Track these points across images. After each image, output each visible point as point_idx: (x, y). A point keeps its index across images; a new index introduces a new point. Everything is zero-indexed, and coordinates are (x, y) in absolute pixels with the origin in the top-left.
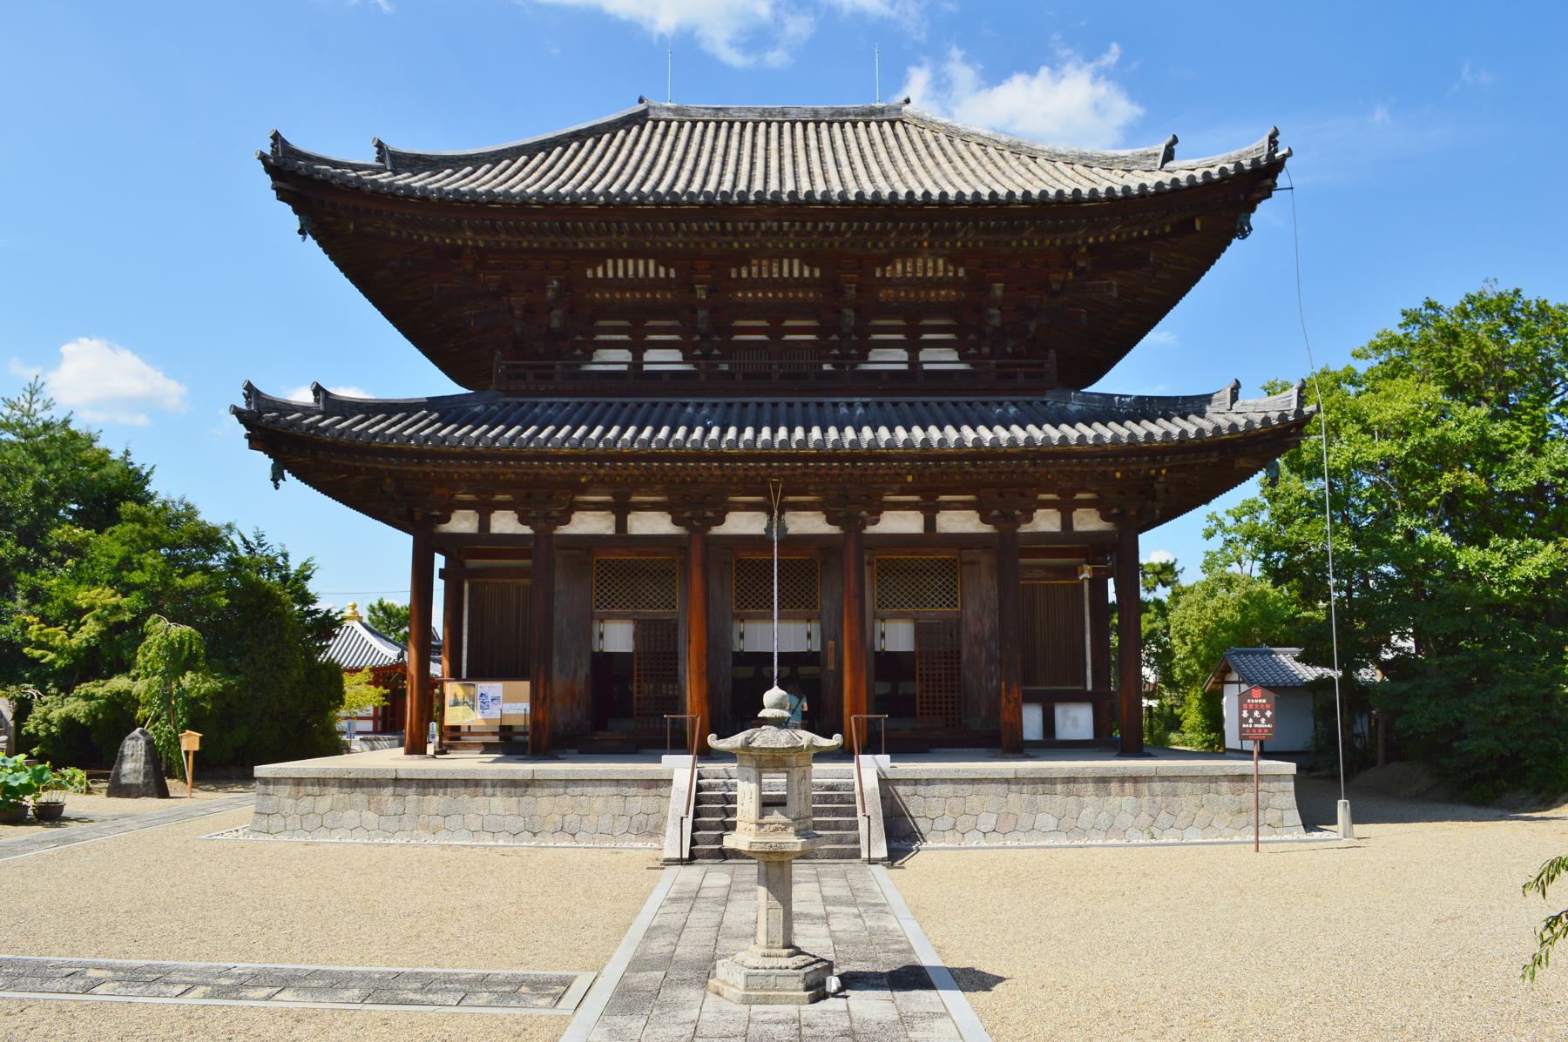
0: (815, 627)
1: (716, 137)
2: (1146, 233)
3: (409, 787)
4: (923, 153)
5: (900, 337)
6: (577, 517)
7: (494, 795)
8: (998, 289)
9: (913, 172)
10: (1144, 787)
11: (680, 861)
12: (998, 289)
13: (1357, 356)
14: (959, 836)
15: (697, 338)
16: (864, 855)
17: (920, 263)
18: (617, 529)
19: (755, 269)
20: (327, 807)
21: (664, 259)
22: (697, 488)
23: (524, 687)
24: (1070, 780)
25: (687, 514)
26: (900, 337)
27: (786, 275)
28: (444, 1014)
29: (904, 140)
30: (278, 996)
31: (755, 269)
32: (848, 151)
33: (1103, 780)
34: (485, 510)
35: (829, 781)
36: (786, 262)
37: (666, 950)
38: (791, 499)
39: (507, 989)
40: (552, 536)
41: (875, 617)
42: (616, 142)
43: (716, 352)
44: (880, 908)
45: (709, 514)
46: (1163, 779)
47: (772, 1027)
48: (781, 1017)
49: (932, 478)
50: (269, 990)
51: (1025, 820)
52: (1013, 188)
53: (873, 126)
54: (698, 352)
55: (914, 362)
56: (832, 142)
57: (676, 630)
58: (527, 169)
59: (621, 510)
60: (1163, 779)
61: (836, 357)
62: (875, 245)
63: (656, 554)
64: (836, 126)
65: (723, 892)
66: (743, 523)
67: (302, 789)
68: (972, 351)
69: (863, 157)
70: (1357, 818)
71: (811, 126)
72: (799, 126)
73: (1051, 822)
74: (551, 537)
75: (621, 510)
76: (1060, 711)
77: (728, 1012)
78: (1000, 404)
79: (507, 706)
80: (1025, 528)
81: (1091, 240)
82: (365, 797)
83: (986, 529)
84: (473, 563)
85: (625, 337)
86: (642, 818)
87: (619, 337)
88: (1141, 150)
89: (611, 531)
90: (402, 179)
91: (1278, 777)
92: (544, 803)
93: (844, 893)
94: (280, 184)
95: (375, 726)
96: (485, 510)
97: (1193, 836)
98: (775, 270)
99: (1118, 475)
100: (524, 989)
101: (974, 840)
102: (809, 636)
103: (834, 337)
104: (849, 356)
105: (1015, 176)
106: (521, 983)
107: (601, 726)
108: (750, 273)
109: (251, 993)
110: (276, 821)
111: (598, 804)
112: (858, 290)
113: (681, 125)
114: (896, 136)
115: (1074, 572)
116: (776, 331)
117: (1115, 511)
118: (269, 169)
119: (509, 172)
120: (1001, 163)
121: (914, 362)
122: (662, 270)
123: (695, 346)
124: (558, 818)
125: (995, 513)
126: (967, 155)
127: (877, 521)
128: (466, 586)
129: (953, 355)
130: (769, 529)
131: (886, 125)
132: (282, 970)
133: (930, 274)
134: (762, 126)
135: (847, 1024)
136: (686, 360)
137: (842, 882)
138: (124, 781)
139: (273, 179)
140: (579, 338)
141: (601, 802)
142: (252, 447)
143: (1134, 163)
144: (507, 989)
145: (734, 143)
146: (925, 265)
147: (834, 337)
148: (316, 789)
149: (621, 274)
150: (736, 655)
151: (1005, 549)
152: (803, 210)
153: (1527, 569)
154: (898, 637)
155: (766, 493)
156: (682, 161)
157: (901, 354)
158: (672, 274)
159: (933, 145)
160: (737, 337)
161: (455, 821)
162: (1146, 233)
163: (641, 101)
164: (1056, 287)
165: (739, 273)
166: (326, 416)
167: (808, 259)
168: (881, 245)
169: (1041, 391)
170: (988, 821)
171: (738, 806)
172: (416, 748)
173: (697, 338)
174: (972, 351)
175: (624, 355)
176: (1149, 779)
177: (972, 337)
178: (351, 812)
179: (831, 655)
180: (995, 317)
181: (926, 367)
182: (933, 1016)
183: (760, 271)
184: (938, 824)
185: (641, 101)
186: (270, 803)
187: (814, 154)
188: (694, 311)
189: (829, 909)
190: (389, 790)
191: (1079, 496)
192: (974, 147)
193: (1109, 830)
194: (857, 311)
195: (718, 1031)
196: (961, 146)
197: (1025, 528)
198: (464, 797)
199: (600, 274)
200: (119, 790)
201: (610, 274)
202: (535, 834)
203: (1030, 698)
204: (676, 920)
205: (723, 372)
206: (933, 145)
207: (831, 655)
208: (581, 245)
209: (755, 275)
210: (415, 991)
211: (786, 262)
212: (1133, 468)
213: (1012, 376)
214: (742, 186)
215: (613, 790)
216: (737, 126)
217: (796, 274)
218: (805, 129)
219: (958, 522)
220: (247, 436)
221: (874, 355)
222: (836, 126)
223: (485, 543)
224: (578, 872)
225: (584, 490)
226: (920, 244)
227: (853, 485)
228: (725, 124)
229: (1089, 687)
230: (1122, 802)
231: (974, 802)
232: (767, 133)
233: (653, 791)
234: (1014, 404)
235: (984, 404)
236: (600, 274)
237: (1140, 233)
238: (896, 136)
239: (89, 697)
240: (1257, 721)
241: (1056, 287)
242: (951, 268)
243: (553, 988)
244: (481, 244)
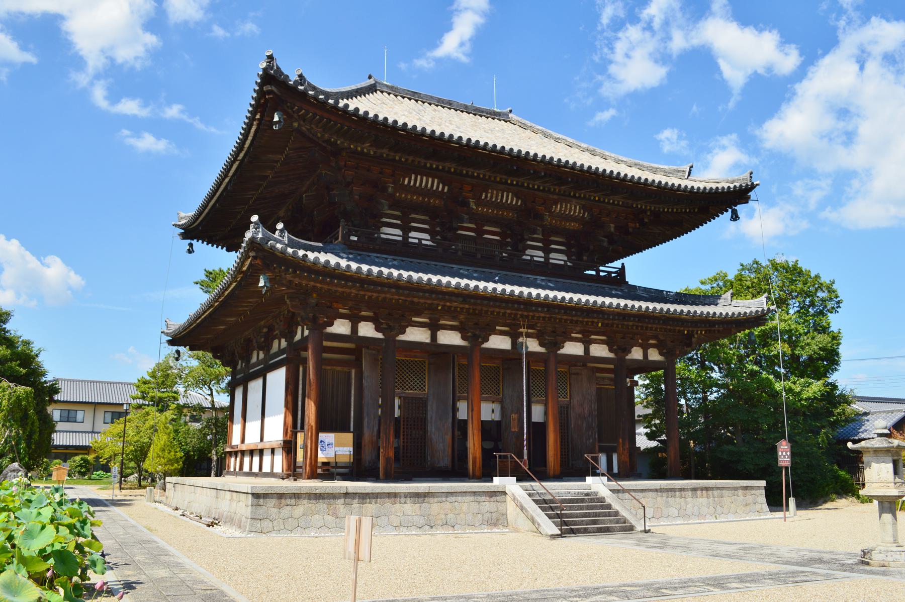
3: (354, 498)
5: (540, 244)
6: (409, 330)
7: (405, 503)
10: (710, 493)
13: (702, 283)
20: (301, 513)
23: (349, 437)
24: (682, 490)
26: (540, 244)
33: (694, 490)
34: (355, 321)
35: (586, 491)
40: (395, 341)
46: (718, 488)
57: (426, 406)
59: (434, 328)
60: (718, 488)
63: (415, 357)
67: (283, 501)
70: (799, 506)
75: (434, 328)
79: (337, 449)
82: (325, 506)
85: (399, 222)
86: (489, 515)
88: (675, 167)
89: (428, 341)
91: (759, 488)
92: (435, 507)
96: (355, 321)
97: (731, 517)
102: (493, 411)
108: (486, 197)
110: (266, 524)
111: (465, 507)
122: (441, 186)
123: (437, 233)
124: (443, 516)
141: (466, 505)
148: (293, 501)
153: (808, 393)
160: (486, 236)
161: (383, 520)
163: (370, 77)
167: (517, 195)
176: (712, 489)
178: (317, 516)
183: (492, 197)
185: (370, 77)
190: (341, 501)
193: (699, 516)
198: (388, 504)
199: (406, 182)
202: (432, 527)
203: (602, 450)
215: (472, 498)
230: (702, 500)
233: (493, 499)
236: (406, 182)
241: (630, 230)
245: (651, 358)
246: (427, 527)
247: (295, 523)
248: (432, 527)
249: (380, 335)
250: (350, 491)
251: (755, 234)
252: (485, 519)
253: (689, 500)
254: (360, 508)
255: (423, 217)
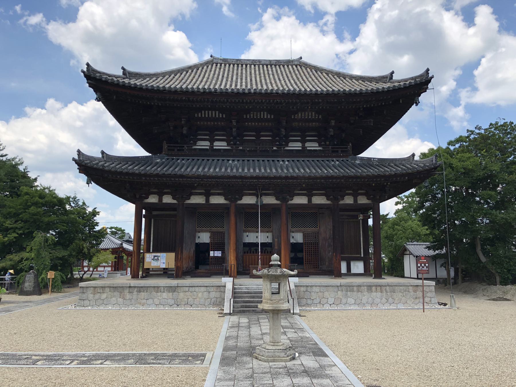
0: (270, 235)
1: (238, 69)
2: (383, 104)
4: (308, 76)
5: (299, 138)
6: (192, 197)
8: (333, 123)
9: (305, 83)
11: (230, 314)
12: (333, 123)
14: (322, 306)
15: (232, 138)
16: (292, 312)
17: (307, 114)
18: (206, 202)
19: (252, 115)
21: (221, 111)
22: (234, 187)
25: (230, 197)
27: (262, 117)
28: (161, 369)
29: (301, 72)
30: (105, 363)
31: (252, 115)
32: (282, 75)
36: (262, 113)
37: (234, 344)
38: (264, 192)
39: (184, 358)
41: (291, 232)
42: (204, 71)
43: (238, 143)
44: (302, 330)
45: (237, 197)
47: (279, 370)
48: (280, 366)
49: (310, 186)
50: (101, 361)
51: (344, 301)
52: (340, 88)
53: (290, 67)
54: (232, 143)
55: (304, 147)
56: (277, 72)
58: (175, 79)
61: (277, 145)
62: (293, 108)
64: (277, 66)
65: (247, 324)
66: (248, 200)
68: (323, 143)
69: (288, 77)
71: (269, 66)
72: (265, 66)
73: (353, 302)
74: (183, 204)
75: (208, 195)
76: (352, 264)
77: (262, 365)
78: (333, 161)
80: (341, 202)
81: (365, 106)
83: (329, 202)
84: (155, 213)
85: (208, 137)
87: (205, 137)
89: (204, 202)
90: (133, 82)
93: (288, 324)
94: (89, 81)
95: (112, 269)
97: (400, 306)
98: (259, 115)
99: (374, 185)
100: (190, 358)
101: (327, 307)
102: (268, 237)
103: (277, 138)
104: (282, 145)
105: (339, 84)
106: (189, 356)
107: (197, 268)
108: (250, 116)
109: (95, 362)
110: (87, 302)
112: (286, 123)
113: (225, 65)
114: (298, 70)
115: (357, 217)
116: (258, 136)
117: (372, 197)
118: (86, 76)
119: (169, 80)
120: (334, 80)
121: (304, 147)
122: (221, 115)
124: (186, 300)
125: (332, 197)
126: (322, 77)
127: (292, 200)
128: (152, 220)
129: (317, 145)
130: (257, 202)
131: (294, 66)
132: (103, 354)
133: (310, 117)
134: (253, 66)
135: (303, 368)
136: (228, 145)
137: (286, 321)
138: (25, 289)
139: (87, 80)
140: (192, 137)
142: (80, 172)
143: (379, 80)
144: (184, 358)
145: (244, 72)
146: (308, 114)
147: (277, 138)
149: (207, 116)
150: (244, 244)
151: (333, 210)
152: (269, 95)
154: (298, 237)
155: (256, 190)
156: (227, 78)
157: (299, 144)
158: (224, 116)
159: (311, 73)
160: (262, 138)
161: (150, 301)
162: (383, 104)
164: (352, 122)
165: (247, 116)
166: (106, 162)
167: (270, 112)
168: (295, 107)
169: (347, 156)
170: (331, 301)
171: (263, 295)
172: (135, 276)
173: (232, 138)
174: (323, 143)
175: (207, 143)
177: (323, 138)
178: (114, 299)
179: (276, 244)
180: (332, 132)
181: (308, 148)
182: (331, 366)
183: (253, 116)
184: (315, 301)
186: (84, 296)
187: (271, 76)
188: (231, 129)
189: (285, 330)
191: (360, 192)
192: (324, 74)
194: (285, 129)
195: (260, 371)
196: (320, 74)
197: (341, 202)
199: (200, 116)
200: (23, 293)
201: (203, 116)
202: (178, 305)
203: (343, 259)
204: (235, 334)
205: (240, 150)
206: (311, 73)
207: (276, 244)
208: (194, 106)
209: (252, 117)
210: (152, 359)
211: (262, 113)
212: (379, 182)
213: (337, 151)
214: (249, 87)
216: (244, 66)
217: (265, 117)
218: (267, 67)
219: (319, 200)
220: (78, 169)
221: (290, 144)
222: (277, 66)
223: (161, 207)
224: (191, 321)
225: (195, 188)
226: (308, 107)
227: (284, 187)
228: (240, 65)
229: (362, 256)
230: (376, 295)
231: (326, 294)
232: (255, 69)
234: (338, 161)
235: (328, 161)
236: (200, 116)
237: (382, 104)
238: (298, 70)
239: (11, 260)
240: (423, 267)
242: (317, 115)
243: (200, 357)
244: (160, 105)
245: (359, 202)
246: (175, 305)
247: (101, 302)
248: (178, 305)
249: (175, 202)
250: (132, 285)
251: (18, 158)
252: (212, 301)
253: (366, 293)
254: (138, 294)
255: (222, 133)
